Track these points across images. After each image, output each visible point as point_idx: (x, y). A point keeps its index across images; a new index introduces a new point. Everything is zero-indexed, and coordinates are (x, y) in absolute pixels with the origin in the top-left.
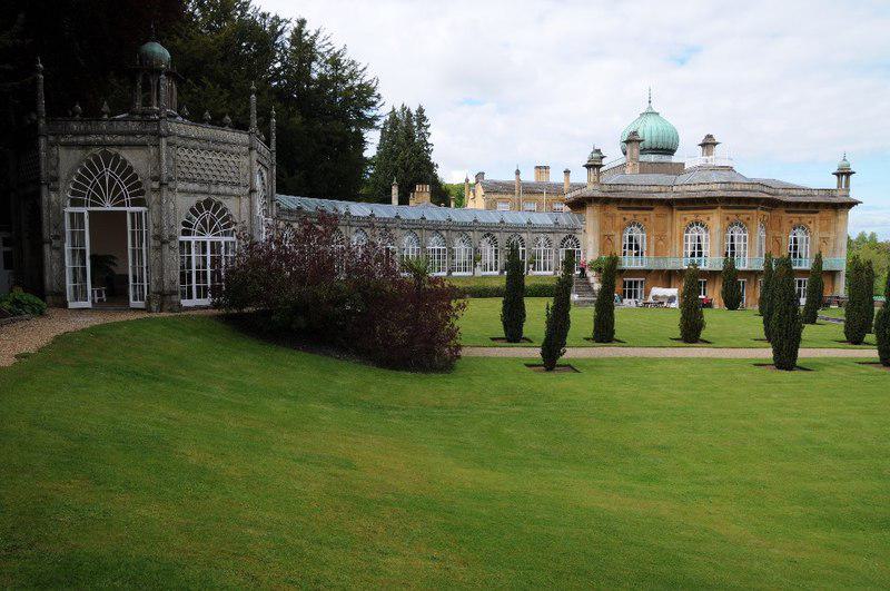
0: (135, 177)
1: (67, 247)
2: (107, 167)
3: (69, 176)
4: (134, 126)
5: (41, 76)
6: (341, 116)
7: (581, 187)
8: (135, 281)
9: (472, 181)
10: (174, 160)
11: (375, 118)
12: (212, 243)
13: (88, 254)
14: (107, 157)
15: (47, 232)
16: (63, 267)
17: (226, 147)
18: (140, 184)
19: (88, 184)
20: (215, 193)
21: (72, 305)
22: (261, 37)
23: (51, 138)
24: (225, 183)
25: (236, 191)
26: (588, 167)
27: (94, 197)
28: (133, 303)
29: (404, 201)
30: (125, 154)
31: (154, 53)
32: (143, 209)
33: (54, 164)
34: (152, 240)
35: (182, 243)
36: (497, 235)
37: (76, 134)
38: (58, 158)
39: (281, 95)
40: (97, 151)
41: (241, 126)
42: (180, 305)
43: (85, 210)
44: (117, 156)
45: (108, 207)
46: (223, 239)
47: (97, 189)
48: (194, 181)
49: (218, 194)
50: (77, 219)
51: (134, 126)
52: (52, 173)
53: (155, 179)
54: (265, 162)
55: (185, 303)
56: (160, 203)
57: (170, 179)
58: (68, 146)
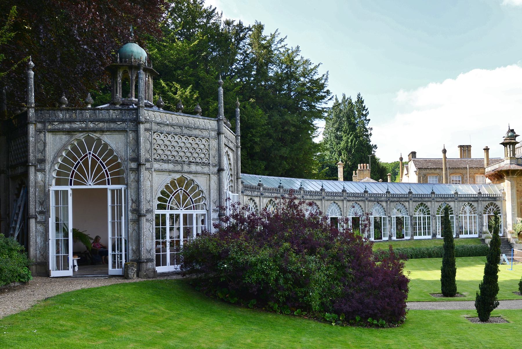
0: (115, 158)
1: (52, 221)
2: (90, 149)
3: (55, 158)
4: (113, 114)
5: (32, 73)
6: (295, 109)
7: (498, 161)
8: (113, 250)
9: (406, 159)
10: (151, 143)
11: (322, 111)
12: (185, 216)
13: (70, 228)
14: (90, 141)
15: (33, 208)
16: (46, 239)
17: (197, 132)
18: (119, 165)
19: (79, 155)
20: (189, 171)
21: (54, 273)
22: (224, 40)
23: (39, 126)
24: (197, 163)
25: (206, 169)
26: (484, 149)
27: (77, 176)
28: (111, 270)
29: (348, 177)
30: (106, 138)
31: (132, 52)
32: (123, 187)
33: (41, 148)
34: (130, 213)
35: (157, 216)
36: (429, 204)
37: (62, 122)
38: (45, 144)
39: (245, 92)
40: (81, 136)
41: (213, 114)
42: (155, 271)
43: (68, 188)
44: (99, 140)
45: (90, 185)
46: (194, 212)
47: (81, 170)
48: (168, 161)
49: (190, 173)
50: (61, 196)
51: (113, 114)
52: (39, 156)
53: (133, 160)
54: (231, 145)
55: (160, 269)
56: (138, 181)
57: (147, 160)
58: (53, 131)
